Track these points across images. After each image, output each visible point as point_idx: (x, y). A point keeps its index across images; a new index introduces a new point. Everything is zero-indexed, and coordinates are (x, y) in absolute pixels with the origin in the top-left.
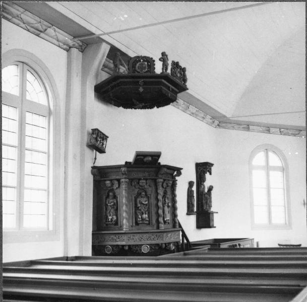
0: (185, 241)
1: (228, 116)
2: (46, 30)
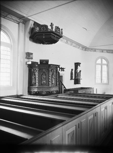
0: (65, 89)
1: (88, 47)
2: (7, 16)
